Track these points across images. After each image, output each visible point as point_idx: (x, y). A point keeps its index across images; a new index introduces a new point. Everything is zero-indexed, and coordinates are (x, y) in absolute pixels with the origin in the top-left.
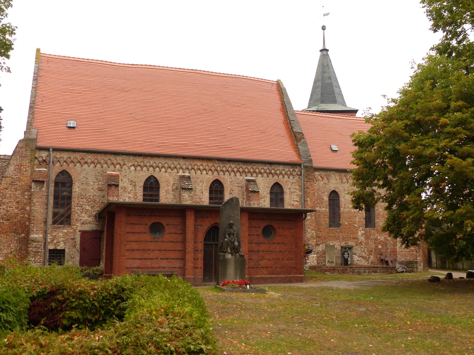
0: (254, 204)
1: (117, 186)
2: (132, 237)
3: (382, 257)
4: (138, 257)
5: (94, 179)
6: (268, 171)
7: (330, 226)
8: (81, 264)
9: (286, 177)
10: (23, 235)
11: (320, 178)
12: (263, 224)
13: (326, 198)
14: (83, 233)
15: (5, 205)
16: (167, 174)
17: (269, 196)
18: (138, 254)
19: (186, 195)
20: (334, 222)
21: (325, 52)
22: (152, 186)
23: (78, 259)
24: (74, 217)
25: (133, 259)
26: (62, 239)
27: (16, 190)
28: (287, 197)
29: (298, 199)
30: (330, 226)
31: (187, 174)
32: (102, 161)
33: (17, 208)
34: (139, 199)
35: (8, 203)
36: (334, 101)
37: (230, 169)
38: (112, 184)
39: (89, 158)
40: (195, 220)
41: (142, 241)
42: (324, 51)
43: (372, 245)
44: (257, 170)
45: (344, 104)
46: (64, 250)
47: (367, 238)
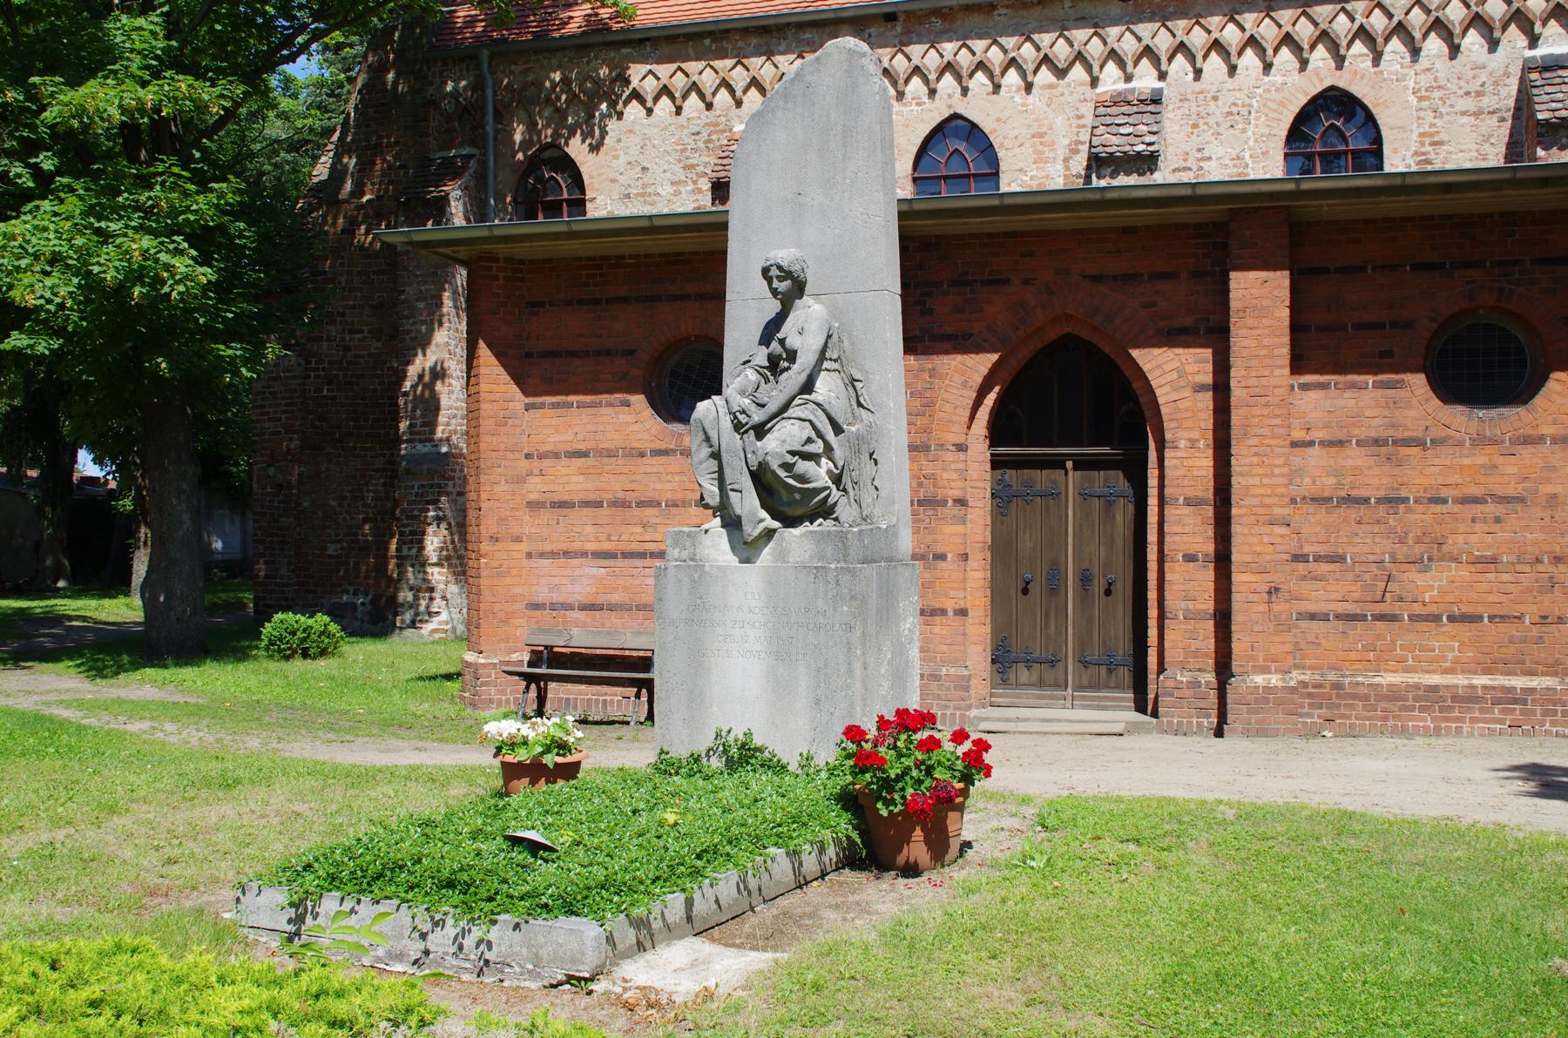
4: (592, 546)
5: (678, 168)
15: (333, 322)
18: (589, 529)
25: (567, 554)
31: (1145, 79)
35: (343, 314)
41: (611, 454)
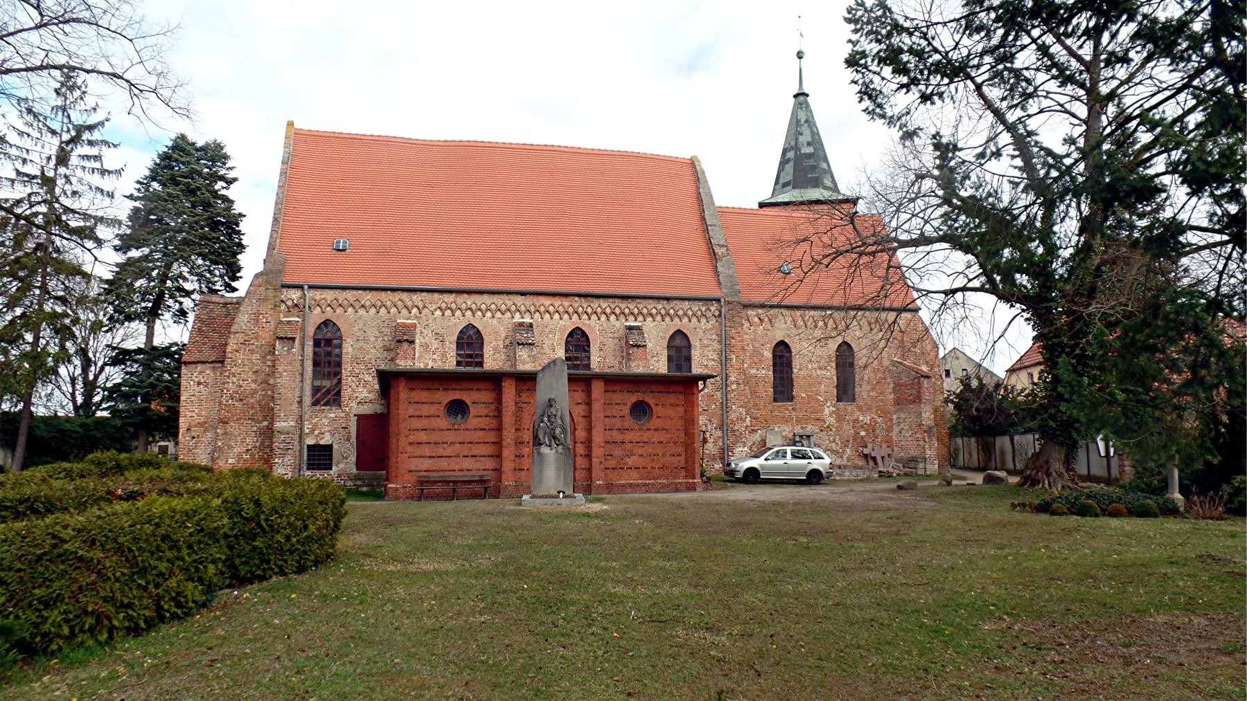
0: (638, 366)
1: (413, 342)
2: (417, 424)
3: (866, 451)
6: (663, 312)
7: (775, 400)
8: (359, 466)
9: (694, 319)
10: (265, 423)
11: (756, 320)
12: (633, 398)
13: (768, 354)
14: (361, 418)
16: (495, 321)
17: (665, 352)
19: (523, 353)
20: (845, 392)
21: (801, 98)
22: (470, 341)
23: (354, 459)
24: (346, 393)
26: (328, 428)
27: (252, 351)
28: (696, 354)
29: (715, 357)
30: (775, 400)
31: (528, 320)
32: (389, 304)
33: (255, 381)
34: (450, 364)
36: (816, 183)
37: (599, 310)
38: (403, 338)
39: (368, 297)
40: (519, 392)
42: (801, 96)
43: (849, 431)
44: (645, 311)
45: (835, 189)
46: (331, 446)
47: (840, 419)
